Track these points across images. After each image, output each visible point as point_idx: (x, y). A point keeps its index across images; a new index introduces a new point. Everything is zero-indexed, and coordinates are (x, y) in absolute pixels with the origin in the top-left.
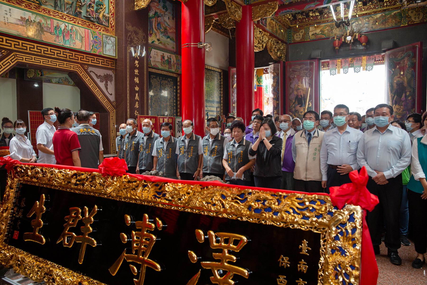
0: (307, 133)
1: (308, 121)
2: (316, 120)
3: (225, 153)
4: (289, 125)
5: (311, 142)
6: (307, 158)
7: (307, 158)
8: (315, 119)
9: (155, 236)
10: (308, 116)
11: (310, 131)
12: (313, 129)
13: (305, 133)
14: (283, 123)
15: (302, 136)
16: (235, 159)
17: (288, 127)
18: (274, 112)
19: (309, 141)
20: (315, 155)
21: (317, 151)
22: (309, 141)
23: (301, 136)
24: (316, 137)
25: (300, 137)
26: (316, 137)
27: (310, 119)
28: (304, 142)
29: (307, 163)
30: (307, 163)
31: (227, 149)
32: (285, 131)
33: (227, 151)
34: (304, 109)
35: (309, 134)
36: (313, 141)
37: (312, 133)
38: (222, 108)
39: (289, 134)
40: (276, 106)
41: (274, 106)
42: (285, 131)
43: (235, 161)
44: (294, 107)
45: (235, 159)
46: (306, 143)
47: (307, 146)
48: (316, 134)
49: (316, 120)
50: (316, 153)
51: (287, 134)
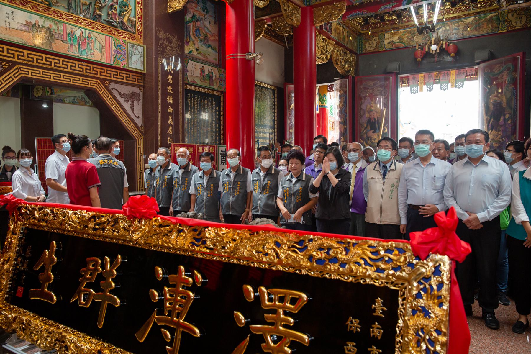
0: (382, 165)
1: (383, 151)
2: (393, 149)
3: (280, 190)
4: (359, 156)
5: (387, 176)
6: (382, 196)
7: (382, 196)
8: (391, 148)
9: (193, 293)
10: (383, 144)
11: (385, 163)
12: (389, 160)
13: (380, 165)
14: (352, 152)
15: (376, 169)
16: (293, 197)
17: (358, 158)
18: (340, 139)
19: (384, 176)
20: (392, 192)
21: (394, 187)
22: (384, 176)
23: (374, 169)
24: (393, 170)
25: (373, 171)
26: (393, 170)
27: (386, 148)
28: (378, 176)
29: (381, 202)
30: (381, 202)
31: (282, 185)
32: (355, 163)
33: (283, 188)
34: (378, 136)
35: (385, 167)
36: (389, 175)
37: (388, 165)
38: (276, 134)
39: (359, 167)
40: (343, 132)
41: (341, 131)
42: (355, 163)
43: (293, 200)
44: (366, 133)
45: (293, 197)
46: (381, 177)
47: (382, 181)
48: (393, 167)
49: (393, 149)
50: (392, 190)
51: (356, 167)
